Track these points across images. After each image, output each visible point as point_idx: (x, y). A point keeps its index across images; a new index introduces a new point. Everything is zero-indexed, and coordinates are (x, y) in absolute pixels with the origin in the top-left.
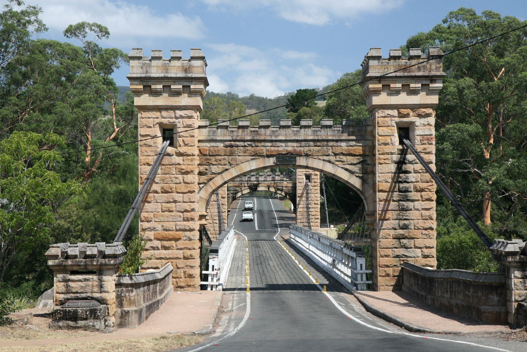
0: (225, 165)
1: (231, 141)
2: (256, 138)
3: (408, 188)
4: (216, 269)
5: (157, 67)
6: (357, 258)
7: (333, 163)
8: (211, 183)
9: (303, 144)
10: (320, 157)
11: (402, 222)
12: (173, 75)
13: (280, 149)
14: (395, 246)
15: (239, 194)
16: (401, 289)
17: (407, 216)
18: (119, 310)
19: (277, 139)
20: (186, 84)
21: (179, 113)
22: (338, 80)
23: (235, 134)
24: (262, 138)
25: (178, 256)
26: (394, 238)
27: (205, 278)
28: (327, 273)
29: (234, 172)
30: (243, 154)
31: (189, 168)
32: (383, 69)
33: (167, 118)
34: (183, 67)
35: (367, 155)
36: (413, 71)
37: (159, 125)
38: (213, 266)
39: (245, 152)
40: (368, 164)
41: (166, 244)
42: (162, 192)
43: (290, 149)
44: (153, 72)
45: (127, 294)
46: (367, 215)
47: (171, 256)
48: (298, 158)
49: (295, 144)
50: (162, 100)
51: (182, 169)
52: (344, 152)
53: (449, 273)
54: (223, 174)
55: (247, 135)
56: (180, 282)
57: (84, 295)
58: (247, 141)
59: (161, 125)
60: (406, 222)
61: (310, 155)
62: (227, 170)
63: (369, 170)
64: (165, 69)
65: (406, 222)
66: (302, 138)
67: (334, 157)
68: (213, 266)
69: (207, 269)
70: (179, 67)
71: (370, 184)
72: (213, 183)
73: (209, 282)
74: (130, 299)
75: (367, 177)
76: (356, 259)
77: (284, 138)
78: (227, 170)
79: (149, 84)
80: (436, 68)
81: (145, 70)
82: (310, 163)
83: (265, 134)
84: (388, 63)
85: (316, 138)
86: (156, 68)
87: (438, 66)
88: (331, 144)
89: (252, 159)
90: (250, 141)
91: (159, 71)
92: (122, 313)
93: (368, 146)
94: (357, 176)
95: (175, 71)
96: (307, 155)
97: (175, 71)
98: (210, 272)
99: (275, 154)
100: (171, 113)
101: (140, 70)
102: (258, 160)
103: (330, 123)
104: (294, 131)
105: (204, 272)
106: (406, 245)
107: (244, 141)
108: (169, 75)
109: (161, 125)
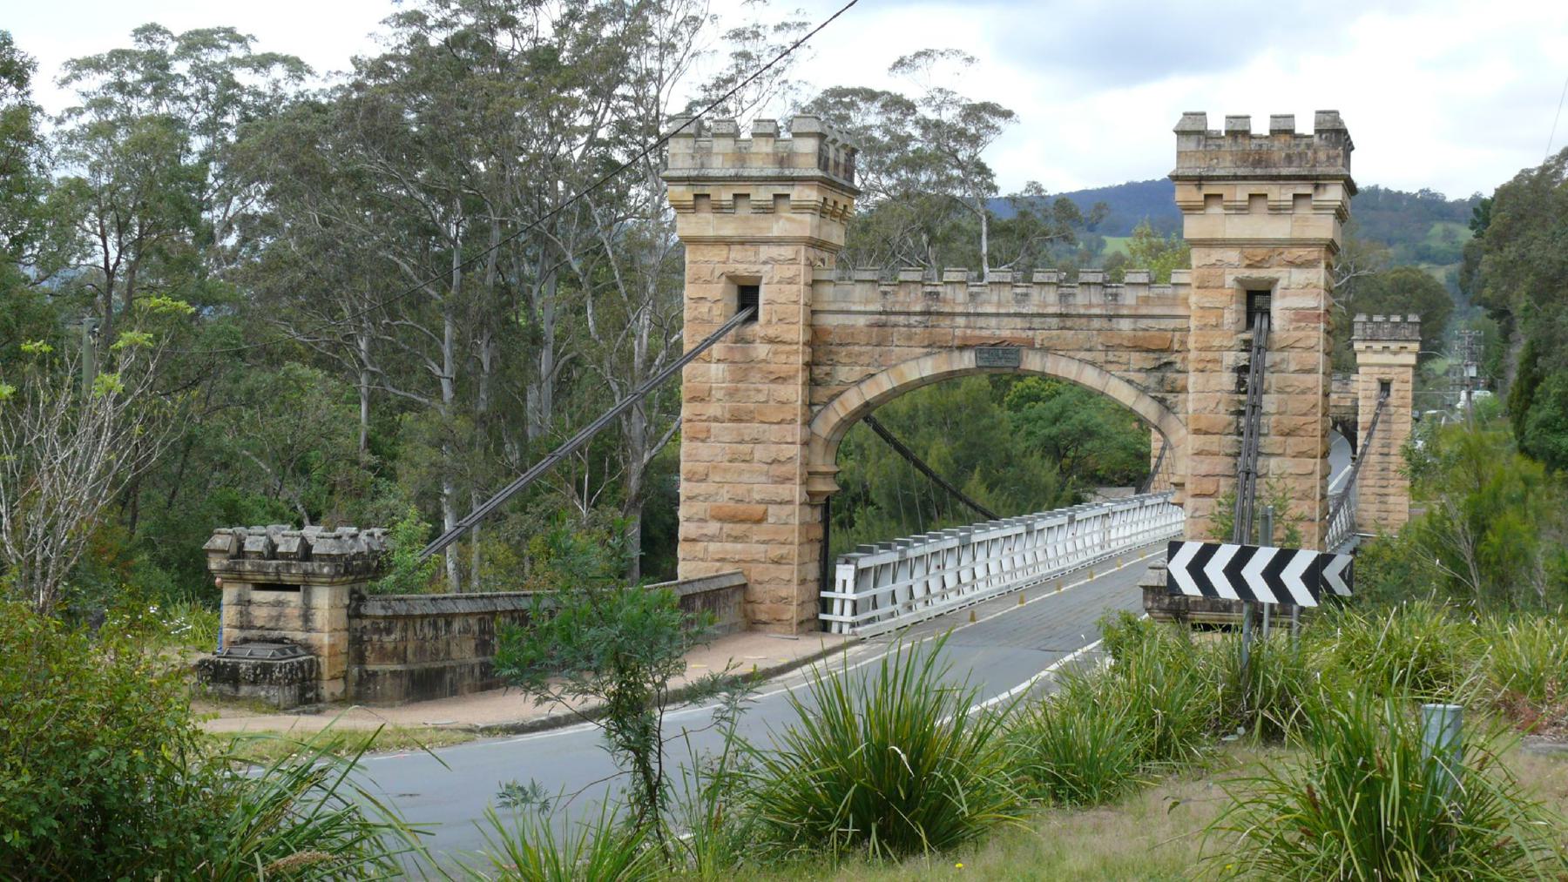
2: (933, 309)
8: (836, 404)
9: (1037, 322)
12: (754, 173)
13: (985, 333)
18: (355, 670)
19: (980, 310)
20: (780, 190)
21: (766, 252)
22: (1035, 187)
23: (890, 298)
24: (947, 309)
29: (885, 383)
31: (784, 370)
33: (743, 263)
34: (775, 154)
36: (1275, 166)
39: (909, 338)
41: (739, 529)
42: (730, 420)
43: (1006, 334)
45: (375, 637)
49: (1018, 322)
50: (728, 228)
52: (1126, 343)
54: (863, 386)
57: (275, 634)
58: (915, 314)
59: (732, 278)
66: (1034, 310)
72: (841, 403)
74: (382, 647)
77: (993, 310)
79: (707, 191)
80: (1328, 157)
85: (1064, 311)
87: (1332, 152)
88: (1096, 323)
89: (928, 354)
90: (922, 313)
92: (360, 675)
95: (760, 164)
96: (1046, 350)
97: (760, 164)
98: (836, 594)
100: (749, 253)
101: (688, 163)
103: (916, 276)
105: (824, 594)
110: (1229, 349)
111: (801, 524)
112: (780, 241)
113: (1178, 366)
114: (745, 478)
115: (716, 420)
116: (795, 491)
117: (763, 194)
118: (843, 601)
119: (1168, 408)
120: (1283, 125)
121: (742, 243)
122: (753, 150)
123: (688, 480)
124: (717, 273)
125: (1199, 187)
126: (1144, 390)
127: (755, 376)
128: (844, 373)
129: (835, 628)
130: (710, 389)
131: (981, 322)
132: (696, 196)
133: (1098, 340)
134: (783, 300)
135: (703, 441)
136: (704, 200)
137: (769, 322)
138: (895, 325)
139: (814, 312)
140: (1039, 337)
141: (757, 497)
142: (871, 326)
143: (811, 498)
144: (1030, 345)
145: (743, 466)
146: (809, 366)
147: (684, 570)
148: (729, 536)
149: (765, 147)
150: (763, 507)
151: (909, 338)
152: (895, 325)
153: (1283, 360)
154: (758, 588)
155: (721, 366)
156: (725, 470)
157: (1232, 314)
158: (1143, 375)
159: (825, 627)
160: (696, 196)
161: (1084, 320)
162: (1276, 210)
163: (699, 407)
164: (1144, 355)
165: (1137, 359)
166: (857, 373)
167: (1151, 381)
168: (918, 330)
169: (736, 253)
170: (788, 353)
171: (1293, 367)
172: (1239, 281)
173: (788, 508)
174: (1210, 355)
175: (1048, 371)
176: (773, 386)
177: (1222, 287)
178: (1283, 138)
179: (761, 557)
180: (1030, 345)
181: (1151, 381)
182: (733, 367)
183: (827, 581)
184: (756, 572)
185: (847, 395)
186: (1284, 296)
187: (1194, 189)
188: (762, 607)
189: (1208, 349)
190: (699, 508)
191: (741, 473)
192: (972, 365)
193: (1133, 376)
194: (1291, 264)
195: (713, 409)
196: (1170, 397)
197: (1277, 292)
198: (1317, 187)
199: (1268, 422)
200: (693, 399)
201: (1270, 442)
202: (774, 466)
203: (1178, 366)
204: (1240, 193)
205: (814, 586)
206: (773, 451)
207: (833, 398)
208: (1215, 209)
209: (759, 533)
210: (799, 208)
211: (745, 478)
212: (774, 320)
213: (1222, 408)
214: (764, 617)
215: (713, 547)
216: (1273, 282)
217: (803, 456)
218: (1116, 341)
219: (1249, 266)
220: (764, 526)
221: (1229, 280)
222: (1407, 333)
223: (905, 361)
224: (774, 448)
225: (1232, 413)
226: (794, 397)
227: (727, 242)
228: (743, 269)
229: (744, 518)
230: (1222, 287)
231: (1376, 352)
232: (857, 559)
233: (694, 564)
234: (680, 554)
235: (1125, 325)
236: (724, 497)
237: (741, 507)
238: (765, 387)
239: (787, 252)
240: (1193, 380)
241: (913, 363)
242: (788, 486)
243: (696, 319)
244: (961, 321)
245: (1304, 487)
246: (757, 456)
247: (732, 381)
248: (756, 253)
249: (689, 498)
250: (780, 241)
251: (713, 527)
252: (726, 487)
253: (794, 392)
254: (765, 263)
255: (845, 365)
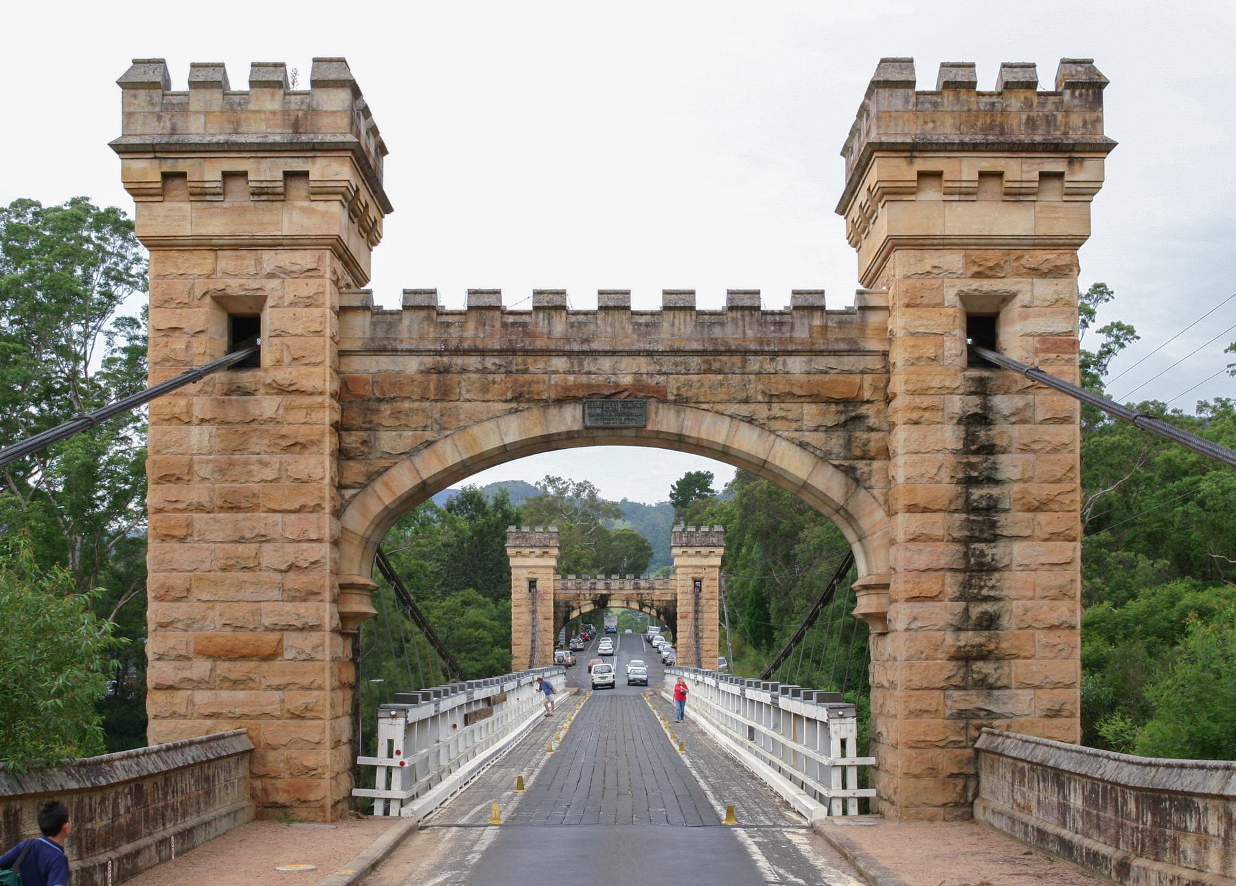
3: (997, 500)
4: (398, 753)
6: (832, 721)
7: (762, 426)
8: (378, 486)
10: (720, 407)
11: (976, 610)
15: (575, 614)
16: (972, 816)
17: (993, 588)
21: (271, 260)
24: (540, 344)
25: (268, 709)
26: (952, 658)
27: (364, 777)
30: (480, 396)
31: (303, 434)
32: (920, 122)
34: (286, 112)
35: (868, 402)
37: (214, 298)
38: (391, 742)
40: (872, 429)
44: (192, 130)
46: (865, 587)
47: (246, 710)
48: (653, 405)
51: (283, 437)
52: (797, 391)
53: (1113, 764)
55: (492, 336)
59: (221, 300)
60: (988, 607)
61: (687, 400)
63: (873, 447)
65: (988, 607)
67: (765, 406)
69: (371, 751)
70: (273, 113)
71: (876, 492)
75: (866, 469)
76: (825, 725)
78: (429, 444)
79: (181, 166)
81: (168, 124)
82: (688, 423)
83: (550, 333)
84: (935, 104)
86: (202, 118)
88: (754, 364)
90: (500, 352)
91: (213, 129)
93: (872, 372)
94: (835, 466)
96: (682, 402)
97: (263, 127)
98: (381, 759)
99: (580, 394)
100: (247, 261)
102: (525, 414)
105: (362, 760)
107: (483, 353)
108: (242, 139)
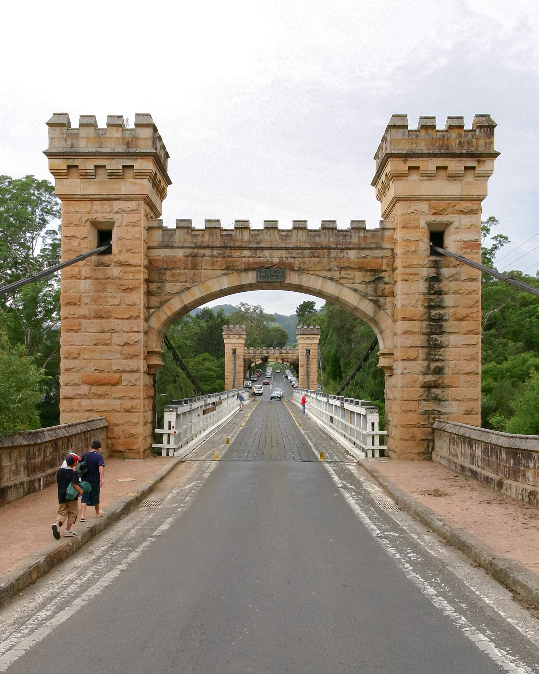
0: (186, 282)
1: (192, 248)
3: (443, 316)
5: (88, 139)
6: (368, 415)
7: (337, 282)
8: (165, 307)
9: (295, 253)
11: (433, 365)
14: (423, 397)
15: (253, 365)
16: (431, 459)
17: (441, 355)
20: (128, 163)
21: (117, 205)
24: (238, 244)
25: (115, 408)
26: (422, 387)
27: (158, 438)
28: (106, 528)
31: (131, 284)
32: (410, 144)
33: (102, 213)
34: (123, 138)
35: (385, 271)
37: (91, 222)
38: (170, 423)
41: (102, 390)
44: (81, 146)
46: (383, 354)
47: (105, 408)
52: (352, 266)
54: (183, 296)
55: (216, 241)
56: (118, 444)
59: (94, 223)
61: (303, 270)
62: (188, 289)
63: (387, 291)
64: (98, 142)
68: (170, 423)
69: (161, 427)
70: (118, 138)
71: (388, 311)
72: (169, 307)
73: (164, 445)
75: (383, 301)
76: (365, 416)
78: (188, 289)
79: (76, 162)
81: (70, 143)
83: (242, 239)
84: (417, 136)
86: (85, 140)
88: (333, 253)
90: (220, 248)
93: (387, 257)
94: (369, 300)
96: (301, 270)
97: (113, 145)
98: (165, 430)
99: (256, 267)
100: (106, 206)
102: (231, 275)
104: (282, 236)
105: (157, 431)
106: (440, 397)
109: (94, 223)
110: (423, 266)
111: (145, 385)
112: (128, 198)
113: (386, 280)
114: (105, 356)
115: (85, 317)
116: (141, 364)
117: (115, 165)
118: (373, 437)
119: (379, 306)
120: (456, 122)
121: (101, 200)
122: (108, 135)
123: (66, 358)
124: (84, 220)
125: (405, 161)
126: (365, 296)
127: (111, 288)
128: (169, 287)
129: (164, 453)
130: (80, 299)
131: (259, 253)
132: (69, 167)
133: (334, 264)
134: (130, 237)
135: (76, 331)
136: (74, 170)
137: (120, 252)
138: (203, 256)
139: (149, 248)
140: (297, 263)
141: (115, 368)
142: (187, 256)
143: (150, 370)
144: (291, 268)
145: (105, 348)
146: (148, 281)
147: (65, 419)
148: (95, 394)
149: (116, 133)
150: (118, 375)
151: (213, 264)
152: (203, 256)
153: (457, 273)
154: (116, 429)
155: (88, 281)
156: (92, 351)
157: (425, 245)
158: (363, 286)
159: (158, 453)
160: (69, 167)
161: (325, 252)
162: (453, 177)
163: (72, 309)
164: (364, 273)
165: (359, 276)
166: (178, 286)
167: (370, 289)
168: (219, 259)
169: (97, 206)
170: (134, 273)
171: (463, 278)
172: (429, 224)
173: (136, 375)
174: (411, 271)
175: (303, 284)
176: (124, 294)
177: (418, 227)
178: (457, 131)
179: (118, 408)
180: (291, 268)
181: (370, 289)
182: (96, 282)
183: (159, 422)
184: (115, 418)
185: (172, 301)
186: (456, 233)
187: (401, 163)
188: (119, 441)
189: (410, 267)
190: (73, 377)
191: (103, 352)
192: (254, 281)
193: (358, 287)
194: (461, 212)
195: (83, 310)
196: (381, 300)
197: (452, 228)
198: (479, 162)
199: (448, 313)
200: (69, 304)
201: (449, 325)
202: (126, 347)
203: (386, 280)
204: (431, 165)
205: (150, 426)
206: (125, 337)
207: (162, 303)
208: (414, 177)
209: (117, 391)
210: (140, 175)
211: (105, 356)
212: (124, 250)
213: (419, 304)
214: (121, 448)
215: (84, 402)
216: (448, 225)
217: (145, 342)
218: (346, 264)
219: (435, 214)
220: (119, 387)
221: (423, 223)
222: (316, 332)
223: (210, 279)
224: (125, 335)
225: (425, 307)
226: (138, 301)
227: (90, 199)
228: (100, 218)
229: (104, 383)
230: (418, 227)
231: (305, 339)
232: (176, 408)
233: (71, 414)
234: (61, 408)
235: (352, 254)
236: (90, 369)
237: (103, 375)
238: (119, 295)
239: (132, 205)
240: (399, 288)
241: (215, 280)
242: (135, 360)
243: (69, 250)
244: (247, 253)
245: (472, 353)
246: (114, 341)
247: (96, 291)
248: (111, 206)
249: (67, 370)
250: (128, 198)
251: (84, 389)
252: (93, 362)
253: (138, 298)
254: (117, 213)
255: (170, 282)
